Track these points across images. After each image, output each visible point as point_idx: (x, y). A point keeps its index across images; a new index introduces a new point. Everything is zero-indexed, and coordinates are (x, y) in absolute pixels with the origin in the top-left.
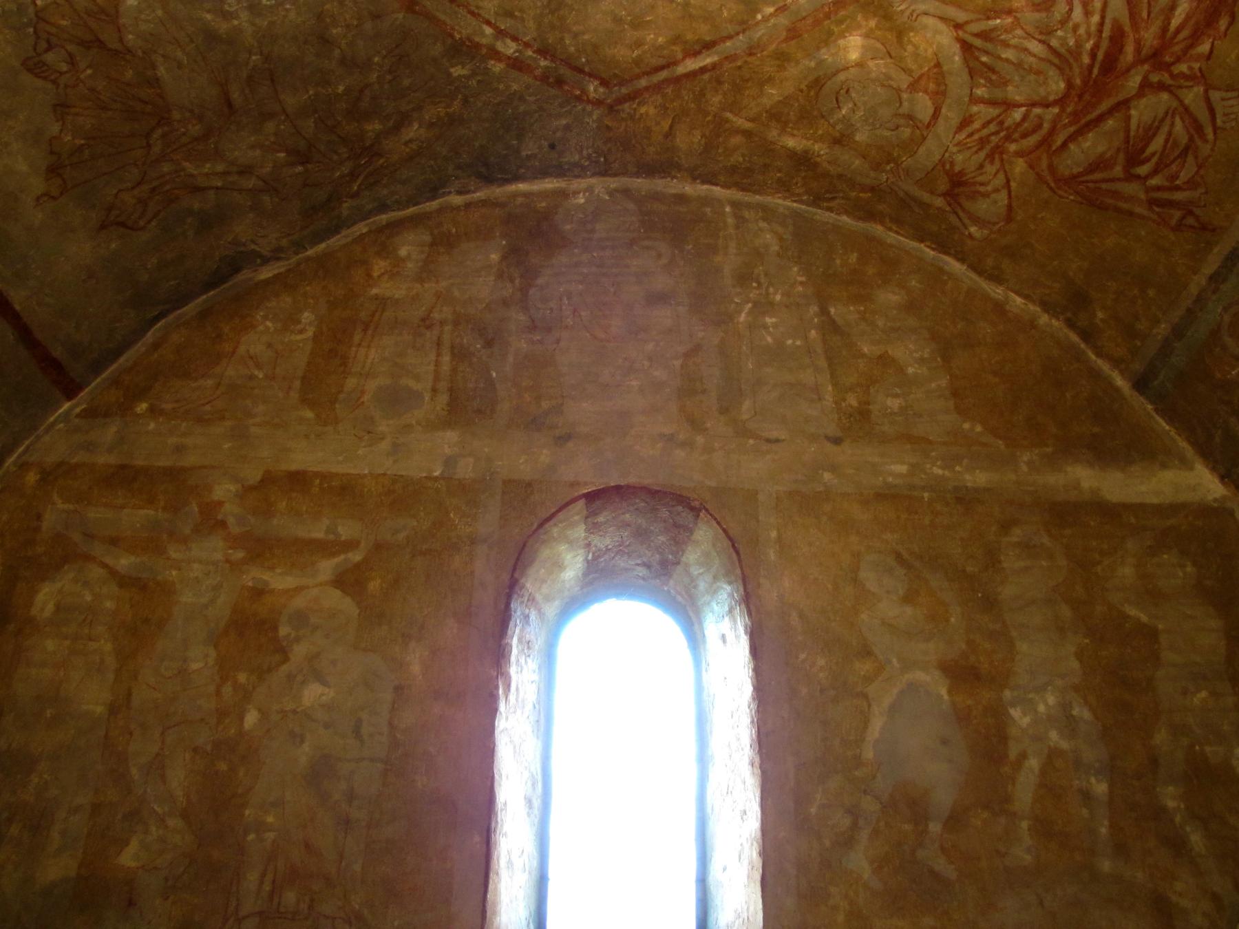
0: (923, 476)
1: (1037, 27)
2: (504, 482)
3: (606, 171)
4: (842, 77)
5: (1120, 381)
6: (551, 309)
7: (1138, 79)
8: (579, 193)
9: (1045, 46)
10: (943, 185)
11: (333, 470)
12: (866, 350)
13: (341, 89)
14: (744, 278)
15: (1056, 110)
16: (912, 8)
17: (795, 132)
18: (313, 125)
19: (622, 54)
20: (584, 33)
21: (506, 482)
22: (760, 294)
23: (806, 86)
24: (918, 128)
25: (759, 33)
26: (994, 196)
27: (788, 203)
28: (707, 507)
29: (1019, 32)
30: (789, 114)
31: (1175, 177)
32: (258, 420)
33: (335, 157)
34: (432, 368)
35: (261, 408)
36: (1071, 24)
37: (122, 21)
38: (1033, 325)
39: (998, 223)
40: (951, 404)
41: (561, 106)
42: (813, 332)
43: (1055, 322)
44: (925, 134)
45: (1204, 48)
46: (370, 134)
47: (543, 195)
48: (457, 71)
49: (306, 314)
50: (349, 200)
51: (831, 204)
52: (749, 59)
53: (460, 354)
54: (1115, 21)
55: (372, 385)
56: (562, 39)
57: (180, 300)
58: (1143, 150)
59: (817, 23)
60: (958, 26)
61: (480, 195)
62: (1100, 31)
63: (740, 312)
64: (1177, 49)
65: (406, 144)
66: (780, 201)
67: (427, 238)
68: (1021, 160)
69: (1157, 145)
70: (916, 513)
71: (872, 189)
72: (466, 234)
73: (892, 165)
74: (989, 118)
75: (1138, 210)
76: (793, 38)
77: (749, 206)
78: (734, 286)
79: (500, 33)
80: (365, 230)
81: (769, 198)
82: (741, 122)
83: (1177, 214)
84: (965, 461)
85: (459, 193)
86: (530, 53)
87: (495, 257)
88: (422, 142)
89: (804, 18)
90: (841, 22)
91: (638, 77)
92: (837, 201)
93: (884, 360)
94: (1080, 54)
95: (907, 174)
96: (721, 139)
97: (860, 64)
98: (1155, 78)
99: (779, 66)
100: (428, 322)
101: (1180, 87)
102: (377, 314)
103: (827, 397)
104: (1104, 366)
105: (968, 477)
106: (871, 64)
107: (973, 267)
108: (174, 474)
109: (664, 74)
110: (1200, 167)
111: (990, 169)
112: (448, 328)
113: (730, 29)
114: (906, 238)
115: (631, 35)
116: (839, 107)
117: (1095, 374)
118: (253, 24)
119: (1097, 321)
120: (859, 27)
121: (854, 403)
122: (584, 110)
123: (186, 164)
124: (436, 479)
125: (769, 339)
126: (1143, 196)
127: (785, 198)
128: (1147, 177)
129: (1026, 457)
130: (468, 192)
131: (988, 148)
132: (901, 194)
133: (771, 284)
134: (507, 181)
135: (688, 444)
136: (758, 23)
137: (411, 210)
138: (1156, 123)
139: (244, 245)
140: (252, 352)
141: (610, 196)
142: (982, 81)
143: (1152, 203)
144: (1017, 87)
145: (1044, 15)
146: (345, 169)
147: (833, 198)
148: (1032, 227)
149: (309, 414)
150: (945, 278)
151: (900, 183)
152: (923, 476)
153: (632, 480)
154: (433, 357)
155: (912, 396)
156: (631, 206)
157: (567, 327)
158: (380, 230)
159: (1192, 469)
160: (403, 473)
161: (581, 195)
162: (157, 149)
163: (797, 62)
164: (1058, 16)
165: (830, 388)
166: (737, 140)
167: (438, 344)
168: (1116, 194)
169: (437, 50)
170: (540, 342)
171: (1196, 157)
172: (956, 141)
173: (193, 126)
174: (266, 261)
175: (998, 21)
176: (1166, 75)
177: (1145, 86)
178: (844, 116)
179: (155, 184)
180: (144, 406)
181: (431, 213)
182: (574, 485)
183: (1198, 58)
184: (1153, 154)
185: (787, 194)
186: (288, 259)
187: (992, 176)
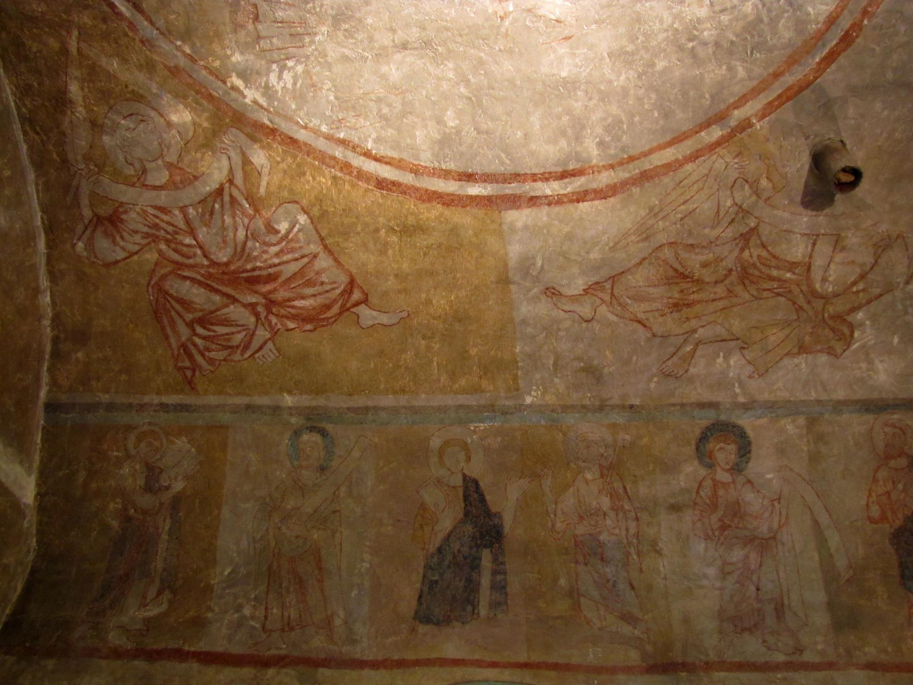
4: (153, 114)
5: (43, 394)
7: (254, 300)
9: (245, 240)
10: (104, 211)
16: (229, 148)
23: (133, 90)
24: (139, 179)
25: (164, 45)
26: (118, 248)
29: (246, 221)
30: (100, 81)
31: (209, 350)
36: (266, 248)
38: (40, 319)
39: (99, 259)
43: (49, 330)
44: (137, 185)
45: (291, 325)
51: (31, 133)
52: (137, 41)
58: (212, 324)
62: (270, 267)
64: (282, 312)
68: (156, 256)
69: (221, 330)
71: (65, 161)
73: (96, 169)
74: (176, 224)
75: (173, 341)
76: (170, 71)
81: (7, 81)
83: (187, 363)
89: (190, 76)
90: (197, 103)
92: (36, 137)
94: (250, 261)
95: (95, 184)
96: (47, 29)
97: (169, 124)
98: (260, 309)
101: (263, 325)
104: (45, 378)
106: (174, 132)
110: (225, 360)
111: (138, 238)
113: (161, 23)
114: (38, 199)
117: (38, 379)
119: (74, 356)
120: (199, 116)
126: (184, 339)
127: (14, 94)
131: (153, 231)
132: (75, 183)
138: (234, 323)
142: (200, 210)
143: (184, 346)
144: (208, 233)
147: (38, 133)
148: (112, 283)
159: (29, 475)
163: (151, 79)
164: (267, 239)
168: (172, 322)
171: (229, 355)
172: (145, 208)
175: (248, 206)
176: (265, 314)
177: (252, 307)
178: (119, 123)
183: (283, 325)
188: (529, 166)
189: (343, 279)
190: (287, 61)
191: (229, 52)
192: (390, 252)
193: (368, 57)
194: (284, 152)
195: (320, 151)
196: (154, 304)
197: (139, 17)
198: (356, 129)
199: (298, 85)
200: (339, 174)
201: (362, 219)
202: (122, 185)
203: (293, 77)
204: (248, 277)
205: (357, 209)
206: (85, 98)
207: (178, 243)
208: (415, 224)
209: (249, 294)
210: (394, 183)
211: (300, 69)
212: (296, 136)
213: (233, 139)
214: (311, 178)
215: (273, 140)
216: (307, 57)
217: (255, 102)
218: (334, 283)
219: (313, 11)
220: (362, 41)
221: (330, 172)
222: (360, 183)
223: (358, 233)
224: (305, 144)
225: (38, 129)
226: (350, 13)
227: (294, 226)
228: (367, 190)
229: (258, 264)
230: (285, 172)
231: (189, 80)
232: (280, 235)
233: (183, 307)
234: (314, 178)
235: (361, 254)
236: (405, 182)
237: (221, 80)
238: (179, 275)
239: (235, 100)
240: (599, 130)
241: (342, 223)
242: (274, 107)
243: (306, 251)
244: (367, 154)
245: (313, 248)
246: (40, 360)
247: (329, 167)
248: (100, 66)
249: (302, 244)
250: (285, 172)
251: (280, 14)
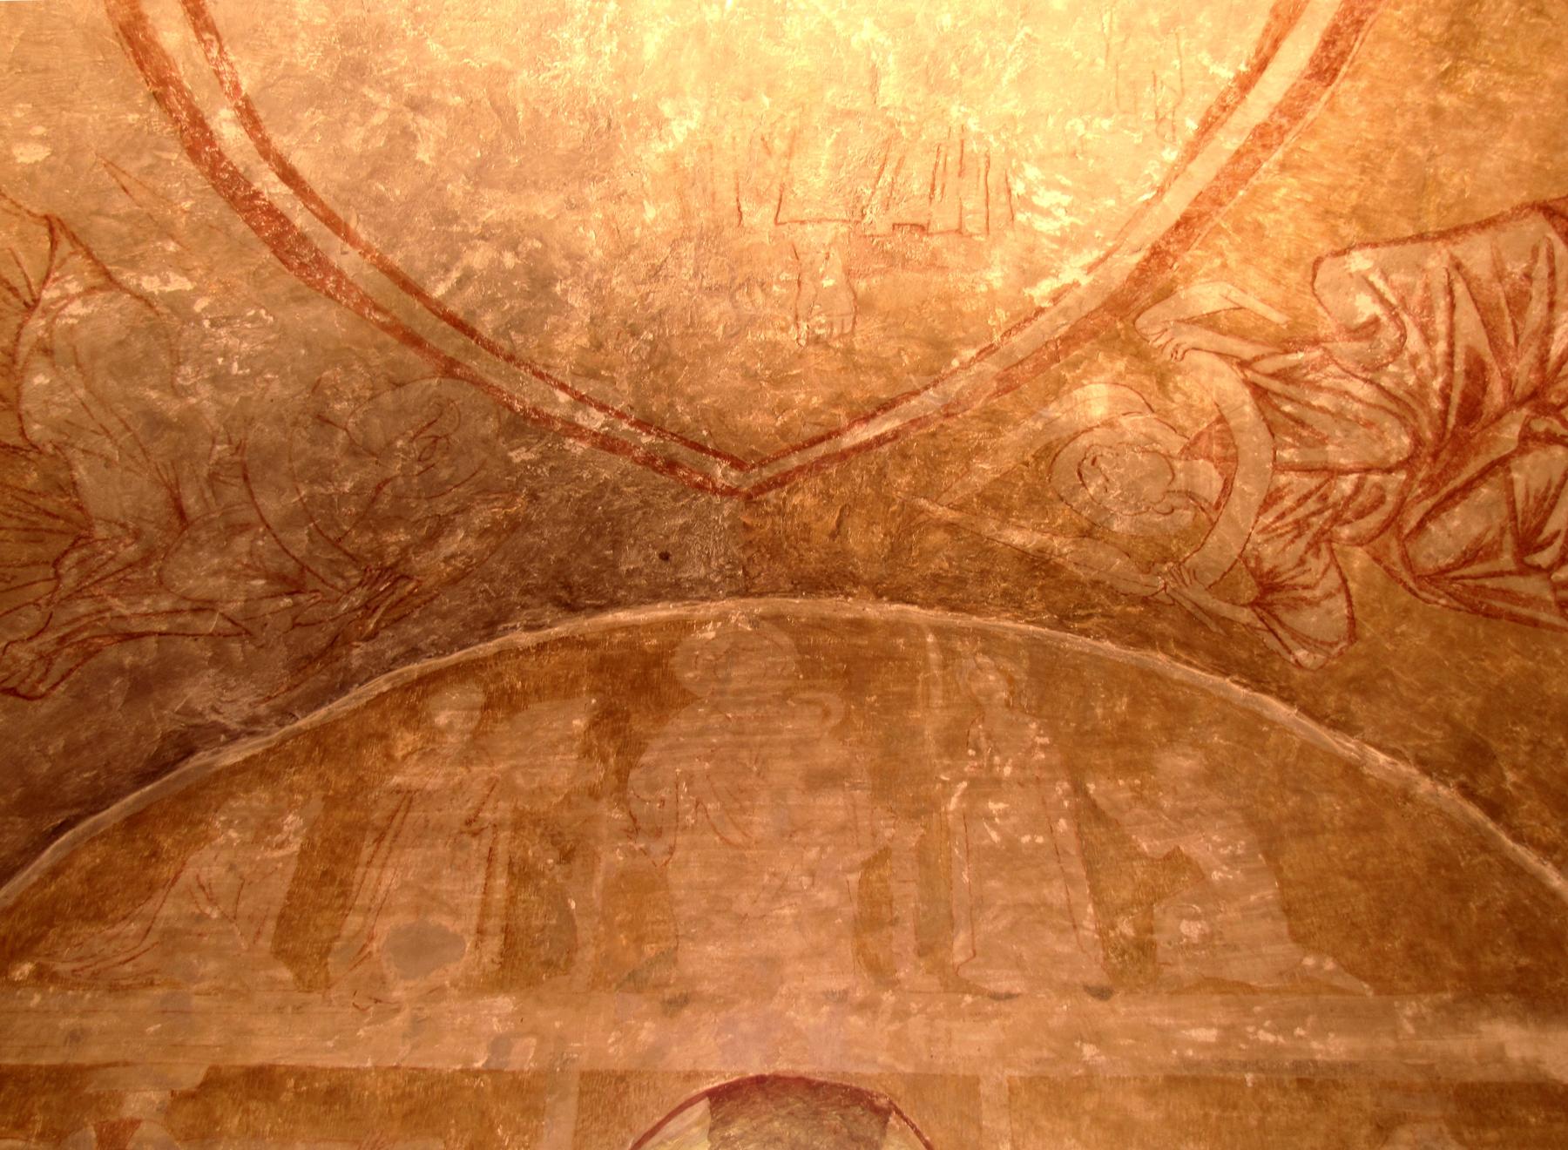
0: (1243, 1046)
1: (1359, 362)
2: (583, 1075)
3: (747, 589)
4: (1083, 441)
6: (663, 801)
7: (1516, 429)
8: (707, 623)
10: (1249, 591)
11: (318, 1064)
12: (1145, 846)
13: (348, 486)
14: (954, 743)
15: (1402, 476)
16: (1176, 341)
17: (1022, 522)
18: (306, 539)
19: (759, 420)
20: (702, 396)
21: (589, 1077)
22: (980, 767)
26: (1325, 603)
27: (1022, 626)
28: (900, 1107)
29: (1333, 369)
30: (1010, 497)
32: (205, 985)
33: (340, 583)
34: (478, 897)
35: (212, 966)
36: (1406, 356)
37: (25, 406)
38: (1406, 795)
40: (1283, 927)
41: (675, 498)
42: (1062, 822)
44: (1214, 518)
46: (391, 549)
47: (652, 627)
48: (519, 456)
49: (290, 818)
50: (362, 645)
51: (1087, 624)
52: (946, 422)
53: (521, 874)
54: (1470, 350)
55: (384, 927)
56: (671, 405)
57: (98, 801)
58: (1539, 530)
59: (1040, 368)
60: (1244, 364)
61: (559, 630)
63: (950, 795)
65: (447, 560)
66: (1010, 624)
67: (479, 698)
68: (1359, 551)
70: (1235, 1107)
71: (1145, 601)
72: (537, 691)
74: (1305, 491)
75: (1544, 617)
76: (1006, 391)
77: (962, 633)
78: (939, 756)
79: (581, 400)
80: (385, 688)
82: (941, 512)
84: (1310, 1020)
85: (528, 628)
86: (625, 426)
87: (579, 723)
88: (471, 558)
89: (1021, 362)
90: (1075, 365)
91: (786, 453)
92: (1095, 620)
93: (1175, 862)
94: (1426, 396)
97: (1109, 424)
98: (1540, 426)
99: (990, 430)
100: (475, 826)
102: (400, 815)
103: (1085, 923)
104: (1529, 857)
105: (1315, 1045)
106: (1125, 422)
107: (1305, 710)
108: (64, 1078)
109: (822, 449)
111: (1316, 565)
112: (505, 834)
113: (915, 381)
114: (1203, 670)
115: (771, 395)
116: (1084, 485)
117: (1515, 871)
118: (218, 402)
119: (1508, 787)
120: (1102, 370)
121: (1129, 931)
122: (709, 503)
123: (115, 602)
124: (477, 1074)
125: (995, 836)
126: (1549, 597)
127: (1016, 619)
128: (1550, 570)
129: (1409, 1009)
130: (540, 627)
131: (1309, 535)
132: (1189, 606)
133: (997, 751)
134: (600, 609)
135: (867, 1007)
136: (954, 372)
137: (457, 656)
138: (1552, 491)
139: (201, 714)
140: (203, 879)
141: (754, 626)
142: (1289, 440)
144: (1340, 445)
145: (1364, 345)
146: (356, 599)
147: (1089, 616)
149: (285, 974)
150: (1265, 729)
151: (1185, 590)
152: (1243, 1046)
153: (782, 1067)
154: (480, 879)
155: (1219, 917)
156: (785, 640)
157: (685, 828)
158: (408, 687)
160: (429, 1065)
161: (710, 626)
162: (69, 582)
163: (1017, 424)
165: (1090, 909)
166: (937, 537)
167: (489, 860)
168: (1506, 594)
169: (491, 425)
170: (645, 852)
172: (1259, 527)
173: (126, 546)
174: (234, 737)
175: (1301, 355)
176: (1556, 423)
177: (1528, 438)
179: (67, 630)
180: (28, 968)
181: (485, 659)
182: (691, 1077)
184: (1556, 534)
185: (1018, 613)
186: (268, 734)
187: (1318, 575)
189: (1533, 228)
190: (1014, 193)
191: (983, 288)
192: (1504, 96)
193: (1027, 35)
194: (1204, 245)
195: (1217, 178)
196: (1455, 604)
197: (903, 407)
198: (1183, 91)
199: (1066, 181)
200: (1278, 155)
201: (1397, 139)
202: (1210, 540)
203: (1048, 189)
204: (1460, 414)
205: (1368, 141)
206: (1036, 528)
207: (1347, 504)
208: (1447, 18)
209: (1498, 429)
210: (1328, 43)
211: (1032, 172)
212: (1176, 216)
213: (1159, 329)
214: (1272, 216)
215: (1175, 259)
216: (1010, 154)
217: (1090, 269)
218: (1535, 251)
219: (915, 128)
220: (989, 42)
221: (1268, 172)
222: (1310, 117)
223: (1432, 156)
224: (1196, 201)
225: (1080, 612)
226: (926, 58)
227: (1371, 285)
228: (1331, 107)
229: (1437, 384)
230: (1247, 261)
231: (1029, 366)
232: (1384, 319)
233: (1482, 560)
234: (1275, 209)
235: (1486, 165)
236: (1330, 16)
237: (1036, 314)
238: (1411, 532)
239: (1080, 302)
241: (1396, 183)
242: (1105, 239)
243: (1439, 280)
244: (1245, 84)
245: (1436, 261)
246: (1484, 844)
247: (1254, 171)
248: (985, 489)
249: (1419, 284)
250: (1247, 261)
251: (915, 186)
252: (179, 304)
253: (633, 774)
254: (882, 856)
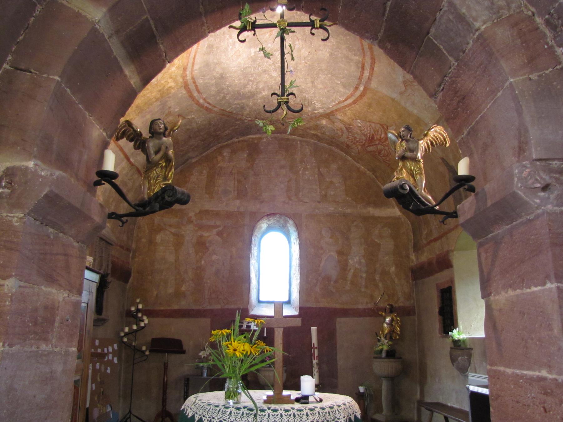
14: (302, 161)
47: (256, 138)
49: (204, 171)
53: (239, 181)
61: (240, 139)
67: (230, 151)
80: (215, 148)
84: (346, 207)
87: (246, 156)
93: (332, 182)
124: (236, 211)
149: (207, 196)
154: (233, 182)
156: (276, 142)
182: (264, 213)
188: (358, 74)
229: (369, 135)
240: (350, 53)
244: (344, 101)
252: (193, 118)
253: (254, 165)
254: (290, 180)
